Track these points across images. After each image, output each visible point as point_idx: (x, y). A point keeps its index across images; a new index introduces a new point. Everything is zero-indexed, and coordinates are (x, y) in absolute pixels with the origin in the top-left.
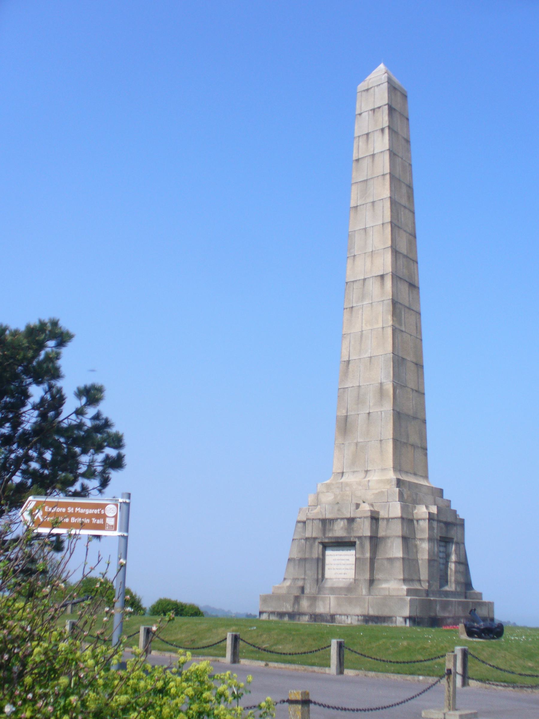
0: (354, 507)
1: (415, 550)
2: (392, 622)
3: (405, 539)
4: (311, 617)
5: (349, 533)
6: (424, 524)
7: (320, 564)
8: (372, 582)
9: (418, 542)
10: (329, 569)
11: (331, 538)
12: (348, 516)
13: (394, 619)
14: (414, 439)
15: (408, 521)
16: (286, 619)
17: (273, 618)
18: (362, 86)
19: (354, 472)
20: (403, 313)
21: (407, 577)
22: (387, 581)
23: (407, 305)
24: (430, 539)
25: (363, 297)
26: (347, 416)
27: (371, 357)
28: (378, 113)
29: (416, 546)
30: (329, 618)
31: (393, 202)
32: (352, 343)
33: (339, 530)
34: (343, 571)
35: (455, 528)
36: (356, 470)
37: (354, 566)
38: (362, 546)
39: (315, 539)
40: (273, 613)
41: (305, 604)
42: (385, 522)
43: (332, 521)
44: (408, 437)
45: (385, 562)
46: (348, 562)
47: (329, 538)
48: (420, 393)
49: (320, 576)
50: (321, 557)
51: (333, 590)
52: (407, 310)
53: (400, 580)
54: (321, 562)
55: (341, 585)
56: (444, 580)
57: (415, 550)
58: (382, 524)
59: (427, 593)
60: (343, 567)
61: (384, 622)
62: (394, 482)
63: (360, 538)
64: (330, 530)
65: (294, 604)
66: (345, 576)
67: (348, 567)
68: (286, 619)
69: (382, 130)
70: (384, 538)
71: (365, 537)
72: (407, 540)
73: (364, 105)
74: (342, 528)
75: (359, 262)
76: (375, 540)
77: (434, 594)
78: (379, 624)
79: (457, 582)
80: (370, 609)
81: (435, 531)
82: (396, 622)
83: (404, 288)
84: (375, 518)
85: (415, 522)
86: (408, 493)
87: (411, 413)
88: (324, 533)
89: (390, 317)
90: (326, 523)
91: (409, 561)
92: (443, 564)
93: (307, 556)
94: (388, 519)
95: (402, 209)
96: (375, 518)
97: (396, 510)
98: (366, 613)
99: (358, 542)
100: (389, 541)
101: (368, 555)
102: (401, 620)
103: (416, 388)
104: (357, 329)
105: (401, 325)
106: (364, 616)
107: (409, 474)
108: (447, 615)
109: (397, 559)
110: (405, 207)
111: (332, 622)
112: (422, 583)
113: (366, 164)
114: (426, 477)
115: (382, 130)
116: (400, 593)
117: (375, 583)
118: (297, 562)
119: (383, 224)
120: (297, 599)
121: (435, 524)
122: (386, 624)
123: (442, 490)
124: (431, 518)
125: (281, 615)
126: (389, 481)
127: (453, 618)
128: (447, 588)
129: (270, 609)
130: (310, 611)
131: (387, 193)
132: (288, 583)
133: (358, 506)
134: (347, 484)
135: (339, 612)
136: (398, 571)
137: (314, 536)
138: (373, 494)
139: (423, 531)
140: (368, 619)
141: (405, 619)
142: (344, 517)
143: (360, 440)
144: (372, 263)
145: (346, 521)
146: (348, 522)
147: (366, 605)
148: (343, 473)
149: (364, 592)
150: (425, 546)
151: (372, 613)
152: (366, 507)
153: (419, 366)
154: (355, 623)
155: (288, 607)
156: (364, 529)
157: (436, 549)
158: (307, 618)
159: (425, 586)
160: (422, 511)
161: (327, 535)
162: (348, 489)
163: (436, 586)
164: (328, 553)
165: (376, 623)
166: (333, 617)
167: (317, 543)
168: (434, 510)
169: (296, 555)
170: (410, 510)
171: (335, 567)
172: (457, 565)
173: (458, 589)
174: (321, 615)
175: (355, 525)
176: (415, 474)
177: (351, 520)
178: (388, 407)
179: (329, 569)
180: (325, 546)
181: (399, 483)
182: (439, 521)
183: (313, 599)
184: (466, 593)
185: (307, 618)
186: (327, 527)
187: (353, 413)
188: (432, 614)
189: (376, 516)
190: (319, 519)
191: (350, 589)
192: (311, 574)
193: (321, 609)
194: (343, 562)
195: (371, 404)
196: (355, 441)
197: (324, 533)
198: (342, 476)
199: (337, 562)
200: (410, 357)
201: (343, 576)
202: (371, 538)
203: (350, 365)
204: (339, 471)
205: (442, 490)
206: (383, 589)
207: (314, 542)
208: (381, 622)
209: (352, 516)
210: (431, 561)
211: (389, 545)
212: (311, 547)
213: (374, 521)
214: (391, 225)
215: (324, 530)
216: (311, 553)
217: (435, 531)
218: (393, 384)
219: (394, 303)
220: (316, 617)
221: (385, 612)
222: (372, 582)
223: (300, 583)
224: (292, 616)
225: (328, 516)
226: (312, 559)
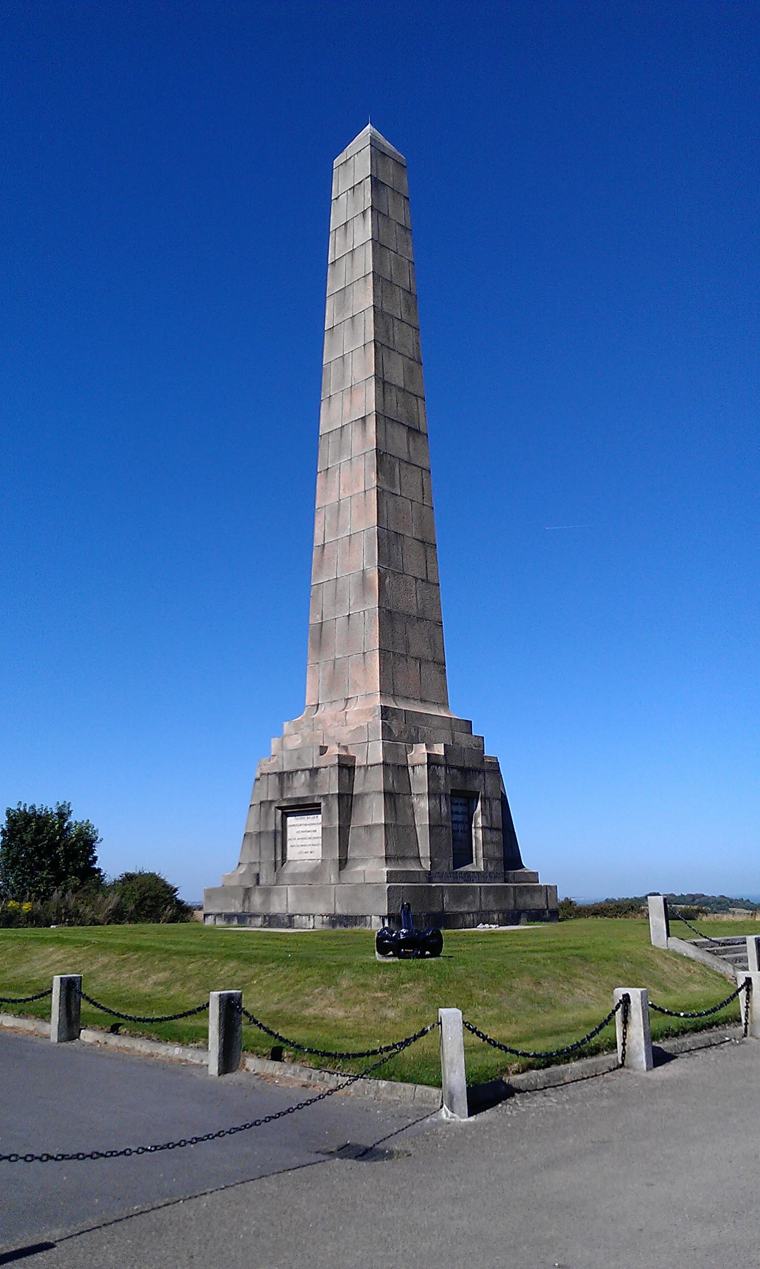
0: (318, 752)
1: (409, 812)
3: (390, 796)
4: (265, 921)
5: (312, 791)
6: (422, 772)
7: (279, 840)
8: (343, 863)
9: (415, 800)
13: (368, 918)
14: (419, 647)
15: (396, 769)
17: (220, 923)
18: (337, 162)
20: (397, 469)
21: (392, 852)
22: (364, 860)
23: (405, 457)
24: (431, 794)
25: (339, 453)
28: (359, 192)
29: (412, 806)
30: (286, 920)
31: (378, 312)
32: (328, 518)
33: (299, 789)
34: (309, 849)
35: (481, 776)
38: (329, 810)
39: (272, 801)
40: (219, 915)
41: (257, 899)
42: (363, 770)
43: (292, 773)
44: (408, 647)
48: (429, 583)
49: (279, 858)
50: (280, 828)
51: (296, 878)
52: (404, 465)
53: (381, 858)
54: (281, 836)
55: (304, 869)
56: (464, 855)
57: (409, 812)
58: (358, 774)
59: (429, 876)
60: (309, 842)
62: (378, 712)
63: (325, 797)
64: (289, 788)
67: (315, 842)
69: (364, 213)
70: (362, 795)
72: (396, 797)
73: (340, 185)
75: (336, 403)
76: (347, 800)
77: (443, 877)
78: (349, 929)
79: (487, 858)
81: (443, 782)
82: (371, 924)
83: (399, 436)
84: (346, 767)
85: (410, 768)
86: (397, 728)
87: (414, 611)
88: (282, 795)
89: (374, 476)
90: (284, 777)
91: (398, 831)
92: (463, 831)
93: (262, 830)
94: (366, 767)
95: (396, 322)
96: (346, 767)
97: (376, 753)
99: (323, 805)
100: (367, 800)
101: (336, 823)
103: (424, 577)
104: (333, 500)
105: (393, 486)
107: (412, 701)
108: (464, 909)
109: (378, 825)
110: (401, 321)
112: (422, 861)
114: (444, 704)
115: (364, 213)
116: (378, 880)
117: (349, 864)
118: (254, 837)
120: (247, 892)
121: (441, 772)
122: (357, 928)
123: (469, 723)
125: (229, 917)
126: (371, 711)
127: (476, 913)
128: (468, 868)
130: (264, 911)
131: (369, 301)
132: (243, 869)
133: (323, 750)
134: (320, 721)
136: (378, 844)
138: (350, 731)
139: (420, 782)
140: (336, 920)
141: (383, 918)
142: (306, 767)
148: (318, 705)
149: (333, 879)
150: (423, 805)
151: (339, 911)
152: (334, 750)
153: (427, 544)
154: (319, 926)
155: (236, 907)
156: (331, 785)
157: (444, 809)
158: (259, 921)
159: (427, 865)
160: (419, 753)
162: (320, 727)
163: (446, 865)
164: (290, 820)
166: (290, 921)
168: (439, 749)
169: (252, 830)
170: (402, 752)
172: (488, 832)
173: (491, 869)
174: (275, 916)
175: (319, 778)
176: (423, 701)
178: (373, 604)
181: (385, 710)
182: (448, 767)
183: (267, 892)
184: (505, 874)
185: (259, 921)
186: (285, 785)
188: (436, 909)
189: (350, 764)
191: (316, 873)
192: (268, 856)
193: (277, 907)
194: (309, 835)
197: (282, 795)
199: (301, 835)
200: (412, 532)
202: (340, 796)
204: (313, 703)
205: (469, 723)
206: (358, 872)
210: (433, 827)
211: (367, 806)
212: (267, 814)
213: (345, 771)
214: (375, 345)
216: (267, 824)
217: (443, 782)
218: (379, 570)
219: (380, 455)
220: (271, 920)
221: (358, 912)
222: (343, 863)
223: (256, 869)
224: (242, 918)
226: (268, 832)
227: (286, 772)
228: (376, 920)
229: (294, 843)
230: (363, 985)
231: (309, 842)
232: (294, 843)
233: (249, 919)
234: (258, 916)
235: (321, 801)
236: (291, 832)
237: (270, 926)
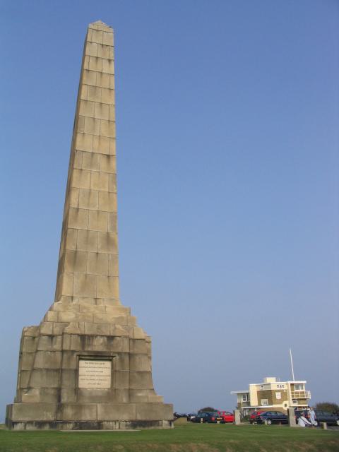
2: (158, 425)
10: (82, 379)
11: (91, 352)
12: (108, 334)
13: (160, 422)
16: (47, 428)
19: (84, 298)
22: (140, 391)
26: (76, 252)
27: (98, 211)
30: (96, 425)
32: (81, 196)
33: (98, 345)
34: (97, 382)
36: (85, 296)
37: (109, 378)
39: (73, 352)
40: (30, 423)
41: (69, 413)
45: (135, 374)
46: (101, 374)
47: (88, 352)
55: (100, 394)
60: (97, 378)
61: (151, 425)
63: (119, 353)
64: (89, 345)
65: (56, 413)
66: (99, 386)
68: (47, 428)
71: (125, 353)
74: (101, 344)
80: (138, 415)
90: (84, 338)
98: (134, 418)
102: (167, 422)
106: (132, 421)
111: (99, 429)
113: (94, 75)
119: (109, 121)
124: (55, 344)
125: (41, 424)
129: (27, 419)
130: (75, 419)
135: (107, 418)
137: (72, 348)
140: (135, 424)
143: (88, 273)
144: (100, 143)
145: (106, 338)
146: (108, 340)
147: (134, 412)
148: (72, 297)
151: (139, 418)
155: (50, 416)
158: (71, 426)
161: (86, 349)
164: (82, 363)
165: (144, 427)
166: (99, 425)
167: (75, 356)
171: (88, 378)
175: (114, 342)
177: (111, 338)
179: (82, 379)
180: (81, 358)
185: (71, 426)
187: (82, 250)
190: (78, 335)
193: (87, 416)
194: (97, 373)
195: (99, 247)
196: (85, 273)
198: (72, 300)
201: (96, 386)
203: (79, 213)
204: (69, 295)
207: (73, 355)
208: (148, 426)
209: (112, 334)
212: (69, 359)
215: (83, 346)
220: (80, 425)
221: (152, 417)
224: (53, 424)
225: (87, 332)
226: (70, 370)
227: (88, 335)
228: (165, 422)
229: (83, 377)
230: (272, 444)
231: (97, 378)
232: (83, 377)
233: (61, 425)
234: (70, 423)
235: (117, 355)
236: (81, 371)
237: (81, 429)
